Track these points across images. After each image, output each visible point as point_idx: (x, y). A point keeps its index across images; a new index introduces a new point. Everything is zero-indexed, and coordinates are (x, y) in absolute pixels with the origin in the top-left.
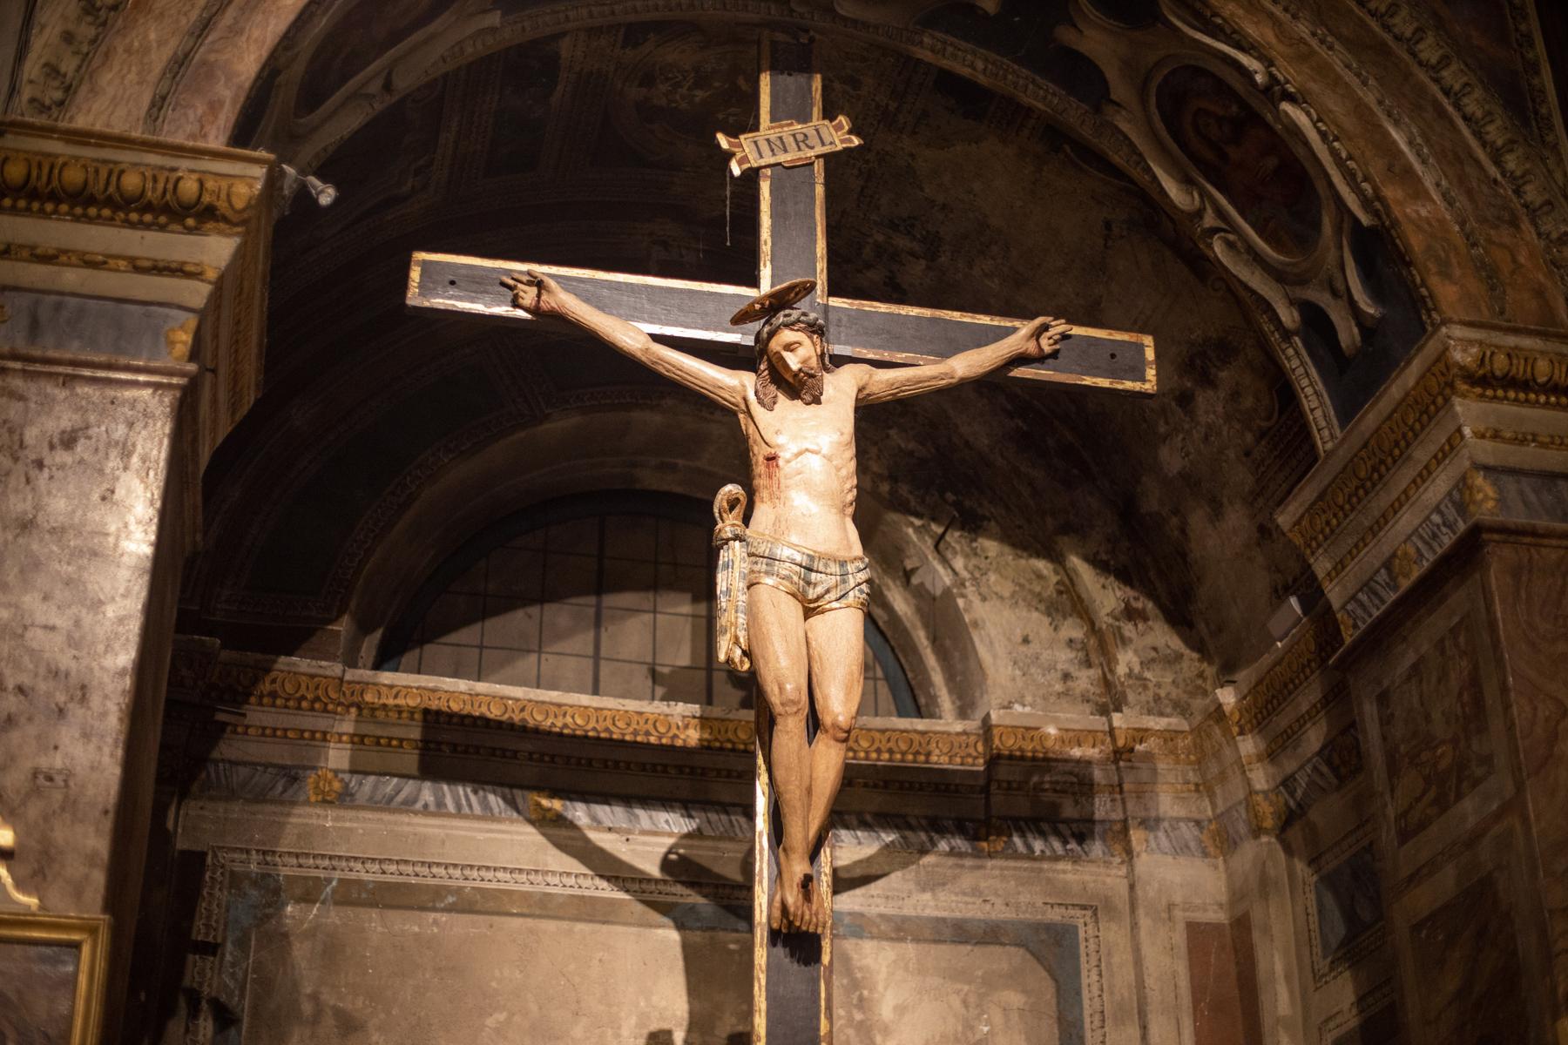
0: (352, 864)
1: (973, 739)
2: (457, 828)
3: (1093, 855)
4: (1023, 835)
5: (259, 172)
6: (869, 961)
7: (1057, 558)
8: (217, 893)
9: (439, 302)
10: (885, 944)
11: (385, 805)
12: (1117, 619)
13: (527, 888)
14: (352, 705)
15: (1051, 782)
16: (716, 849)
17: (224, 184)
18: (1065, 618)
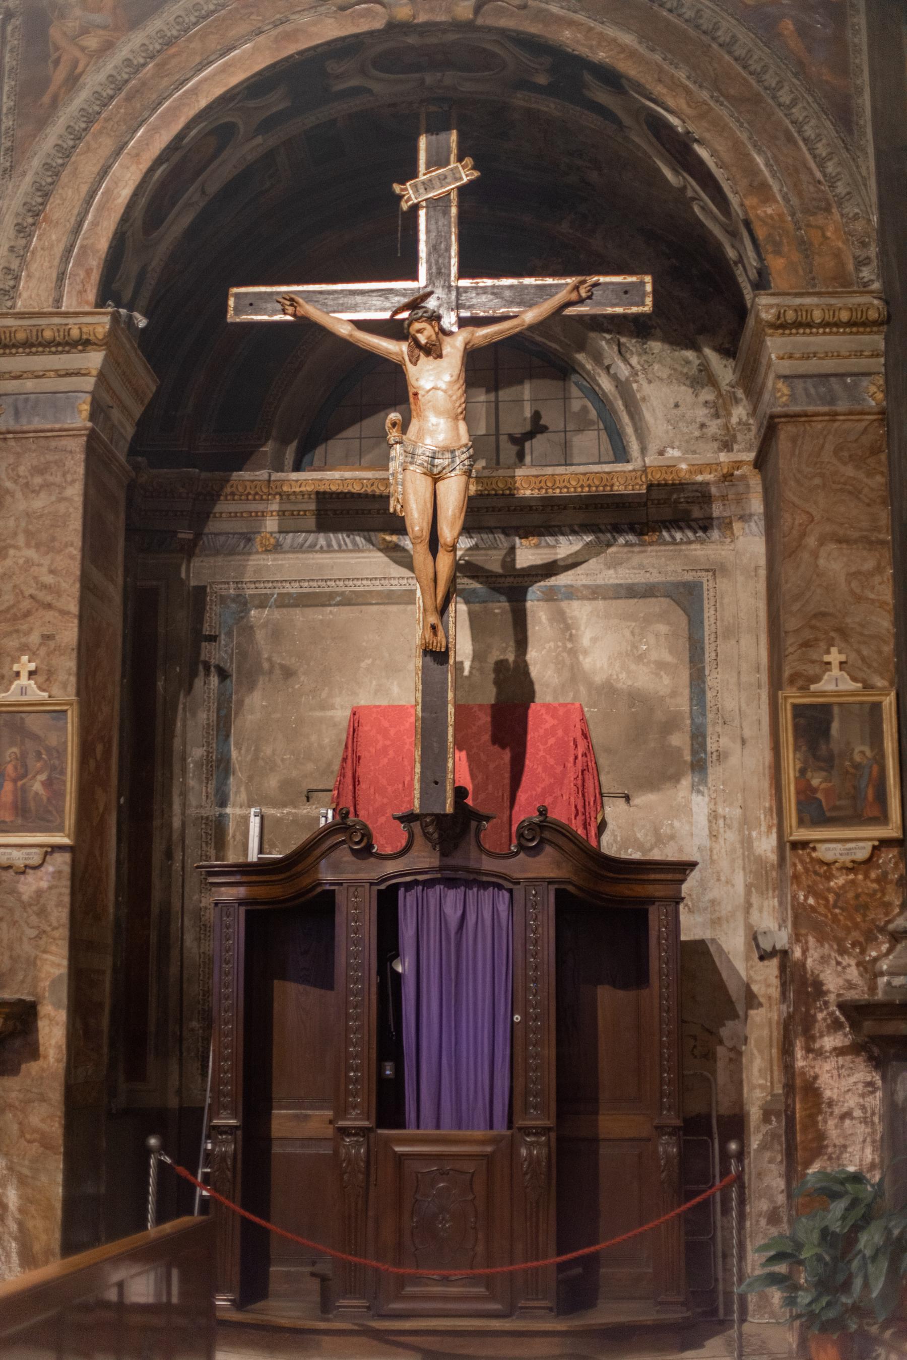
0: (284, 584)
1: (639, 473)
2: (339, 558)
3: (713, 539)
4: (669, 531)
5: (107, 319)
6: (576, 613)
7: (696, 348)
8: (214, 608)
9: (245, 318)
10: (586, 602)
11: (299, 549)
12: (733, 387)
13: (380, 588)
14: (276, 494)
15: (685, 498)
16: (486, 555)
17: (91, 328)
18: (703, 388)
